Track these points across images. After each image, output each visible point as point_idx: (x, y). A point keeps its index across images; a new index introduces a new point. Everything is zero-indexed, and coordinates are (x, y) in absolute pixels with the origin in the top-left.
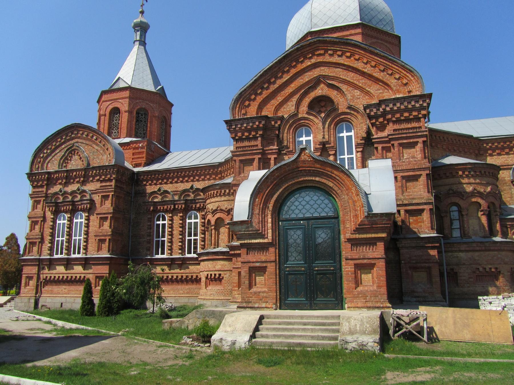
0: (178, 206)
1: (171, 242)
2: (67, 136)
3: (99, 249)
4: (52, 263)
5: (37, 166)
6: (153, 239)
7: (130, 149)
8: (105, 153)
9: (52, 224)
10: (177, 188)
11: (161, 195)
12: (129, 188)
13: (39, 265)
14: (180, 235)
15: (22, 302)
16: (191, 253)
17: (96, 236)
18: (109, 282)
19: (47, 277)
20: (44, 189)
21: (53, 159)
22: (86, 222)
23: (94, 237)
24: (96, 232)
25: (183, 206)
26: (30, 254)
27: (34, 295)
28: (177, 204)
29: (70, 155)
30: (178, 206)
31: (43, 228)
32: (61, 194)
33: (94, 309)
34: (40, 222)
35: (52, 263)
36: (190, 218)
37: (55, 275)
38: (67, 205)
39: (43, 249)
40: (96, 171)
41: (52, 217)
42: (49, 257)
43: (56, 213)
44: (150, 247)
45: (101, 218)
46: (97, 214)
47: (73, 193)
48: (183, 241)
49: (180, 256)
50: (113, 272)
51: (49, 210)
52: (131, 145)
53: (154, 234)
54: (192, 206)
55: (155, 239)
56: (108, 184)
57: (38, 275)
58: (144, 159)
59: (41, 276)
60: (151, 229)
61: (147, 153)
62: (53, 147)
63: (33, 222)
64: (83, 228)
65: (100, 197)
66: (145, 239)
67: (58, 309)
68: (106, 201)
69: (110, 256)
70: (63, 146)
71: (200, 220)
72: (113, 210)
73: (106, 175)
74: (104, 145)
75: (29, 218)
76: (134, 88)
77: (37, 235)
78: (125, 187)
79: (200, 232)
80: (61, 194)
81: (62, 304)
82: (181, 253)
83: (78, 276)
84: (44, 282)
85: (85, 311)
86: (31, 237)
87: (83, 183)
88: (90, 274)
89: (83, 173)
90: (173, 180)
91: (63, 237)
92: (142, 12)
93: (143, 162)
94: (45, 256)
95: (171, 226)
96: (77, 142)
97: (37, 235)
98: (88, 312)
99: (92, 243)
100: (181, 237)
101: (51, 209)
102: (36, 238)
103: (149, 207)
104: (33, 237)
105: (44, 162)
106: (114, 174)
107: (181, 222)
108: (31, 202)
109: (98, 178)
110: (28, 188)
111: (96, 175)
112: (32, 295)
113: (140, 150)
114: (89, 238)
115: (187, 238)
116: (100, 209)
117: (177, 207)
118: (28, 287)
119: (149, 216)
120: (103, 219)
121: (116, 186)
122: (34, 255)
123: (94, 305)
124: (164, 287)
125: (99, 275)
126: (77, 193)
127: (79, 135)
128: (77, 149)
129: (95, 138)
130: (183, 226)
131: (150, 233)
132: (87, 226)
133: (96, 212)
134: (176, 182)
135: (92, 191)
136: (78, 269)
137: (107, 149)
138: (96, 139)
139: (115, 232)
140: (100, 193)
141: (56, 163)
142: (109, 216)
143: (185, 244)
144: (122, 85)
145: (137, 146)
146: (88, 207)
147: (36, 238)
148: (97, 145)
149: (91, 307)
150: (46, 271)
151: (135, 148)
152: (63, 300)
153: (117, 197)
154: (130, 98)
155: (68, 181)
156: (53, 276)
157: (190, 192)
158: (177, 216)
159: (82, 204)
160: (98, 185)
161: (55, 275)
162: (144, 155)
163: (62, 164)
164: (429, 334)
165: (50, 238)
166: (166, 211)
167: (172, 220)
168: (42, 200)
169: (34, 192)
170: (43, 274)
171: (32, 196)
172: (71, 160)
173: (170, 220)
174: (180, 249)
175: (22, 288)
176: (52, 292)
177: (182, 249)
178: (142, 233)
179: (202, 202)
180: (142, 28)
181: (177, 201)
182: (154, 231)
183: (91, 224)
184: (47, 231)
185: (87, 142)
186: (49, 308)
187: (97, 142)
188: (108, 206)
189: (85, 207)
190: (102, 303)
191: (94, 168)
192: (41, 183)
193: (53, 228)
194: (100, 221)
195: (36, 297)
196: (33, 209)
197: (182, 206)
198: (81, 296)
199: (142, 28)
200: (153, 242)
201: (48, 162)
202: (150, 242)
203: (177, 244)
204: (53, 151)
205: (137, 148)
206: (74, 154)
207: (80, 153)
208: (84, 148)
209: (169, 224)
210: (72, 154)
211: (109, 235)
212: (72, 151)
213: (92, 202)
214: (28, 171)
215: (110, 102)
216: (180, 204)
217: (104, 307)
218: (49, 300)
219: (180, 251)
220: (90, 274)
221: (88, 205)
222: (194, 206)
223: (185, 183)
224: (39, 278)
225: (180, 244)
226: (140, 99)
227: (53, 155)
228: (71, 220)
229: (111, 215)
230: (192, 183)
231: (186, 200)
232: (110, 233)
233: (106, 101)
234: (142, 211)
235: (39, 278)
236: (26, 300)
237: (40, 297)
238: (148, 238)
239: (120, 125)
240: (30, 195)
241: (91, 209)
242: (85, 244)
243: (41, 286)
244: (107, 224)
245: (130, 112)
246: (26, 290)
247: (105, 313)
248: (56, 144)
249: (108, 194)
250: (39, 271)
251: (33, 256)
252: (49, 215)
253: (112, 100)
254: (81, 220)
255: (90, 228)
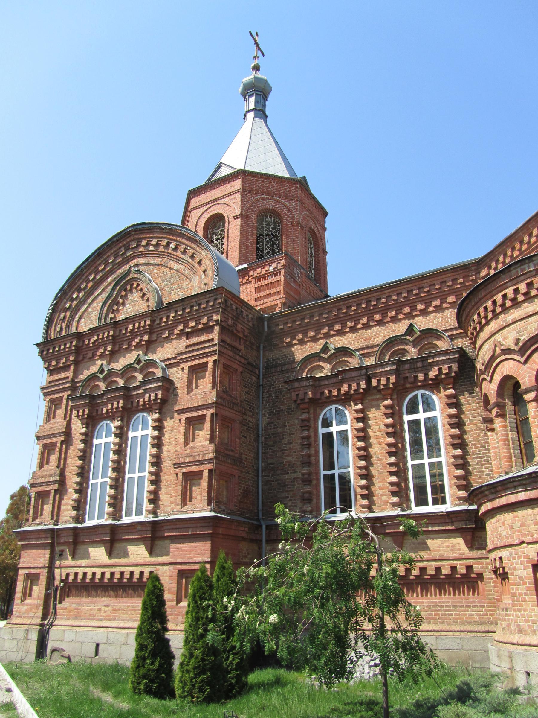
0: (379, 381)
1: (366, 475)
2: (116, 256)
3: (186, 498)
4: (77, 540)
5: (58, 329)
6: (318, 473)
7: (248, 282)
8: (195, 274)
9: (82, 446)
10: (368, 339)
11: (328, 360)
12: (250, 349)
13: (52, 546)
14: (391, 454)
15: (12, 639)
16: (426, 504)
17: (177, 465)
18: (211, 587)
19: (68, 575)
20: (70, 374)
21: (90, 310)
22: (156, 433)
23: (173, 470)
24: (178, 455)
25: (393, 379)
26: (37, 521)
27: (39, 621)
28: (375, 375)
29: (123, 293)
30: (379, 381)
31: (65, 459)
32: (101, 376)
33: (169, 672)
34: (59, 445)
35: (77, 540)
36: (413, 410)
37: (86, 570)
38: (115, 398)
39: (63, 508)
40: (176, 312)
41: (84, 430)
42: (73, 525)
43: (92, 422)
44: (310, 493)
45: (189, 421)
46: (181, 412)
47: (129, 368)
48: (400, 471)
49: (398, 512)
50: (222, 555)
51: (78, 416)
52: (251, 273)
53: (318, 461)
54: (416, 377)
55: (323, 473)
56: (203, 338)
57: (51, 568)
58: (282, 295)
59: (57, 572)
60: (309, 446)
61: (287, 285)
62: (90, 284)
63: (45, 446)
64: (150, 450)
65: (186, 370)
66: (298, 475)
67: (89, 660)
68: (200, 381)
69: (213, 514)
71: (442, 410)
72: (218, 396)
73: (197, 321)
74: (192, 257)
75: (39, 438)
76: (250, 173)
77: (51, 475)
78: (242, 347)
79: (446, 445)
80: (101, 376)
81: (98, 645)
82: (399, 505)
83: (137, 571)
84: (62, 589)
85: (144, 677)
86: (40, 481)
87: (149, 346)
88: (167, 566)
89: (148, 322)
90: (357, 322)
91: (104, 475)
92: (257, 68)
93: (279, 302)
94: (67, 522)
95: (363, 435)
96: (137, 265)
97: (51, 475)
98: (152, 681)
99: (169, 486)
100: (393, 459)
101: (81, 413)
102: (50, 483)
103: (301, 393)
105: (72, 317)
106: (217, 313)
107: (389, 421)
108: (43, 404)
109: (181, 327)
110: (38, 373)
111: (176, 323)
112: (34, 621)
113: (270, 280)
114: (161, 474)
115: (410, 463)
116: (184, 399)
117: (374, 382)
118: (28, 601)
119: (304, 416)
120: (194, 423)
121: (222, 341)
122: (45, 523)
123: (169, 656)
124: (412, 598)
125: (186, 567)
126: (135, 369)
127: (142, 249)
129: (172, 246)
130: (395, 431)
131: (309, 456)
132: (158, 444)
133: (176, 408)
134: (367, 326)
135: (169, 359)
136: (138, 553)
137: (200, 263)
138: (176, 249)
139: (221, 454)
140: (184, 361)
141: (95, 315)
142: (208, 413)
143: (406, 480)
144: (224, 172)
145: (263, 272)
146: (159, 396)
147: (50, 483)
148: (178, 260)
149: (161, 666)
150: (69, 561)
151: (258, 279)
152: (99, 635)
153: (225, 369)
154: (243, 190)
155: (117, 348)
156: (81, 571)
157: (406, 343)
158: (378, 408)
159: (146, 391)
160: (181, 345)
161: (86, 570)
162: (281, 288)
163: (107, 315)
164: (472, 659)
165: (78, 479)
166: (346, 400)
167: (363, 419)
168: (65, 397)
169: (50, 382)
170: (60, 567)
171: (46, 391)
172: (123, 304)
173: (358, 420)
174: (394, 494)
175: (17, 601)
176: (77, 614)
177: (399, 491)
178: (289, 459)
179: (444, 362)
180: (259, 91)
181: (375, 366)
182: (317, 452)
183: (166, 438)
184: (74, 464)
185: (158, 260)
186: (69, 658)
187: (179, 254)
188: (205, 391)
189: (153, 398)
190: (191, 655)
191: (170, 305)
192: (64, 360)
193: (85, 456)
194: (186, 429)
195: (42, 625)
196: (48, 419)
197: (388, 379)
198: (136, 624)
199: (259, 91)
200: (318, 480)
201: (80, 318)
202: (310, 479)
203: (383, 482)
205: (264, 277)
206: (131, 290)
207: (141, 286)
208: (151, 273)
209: (358, 430)
210: (125, 290)
211: (209, 461)
212: (126, 285)
213: (168, 384)
214: (40, 339)
215: (205, 208)
216: (382, 374)
217: (200, 670)
218: (69, 634)
219: (396, 499)
220: (167, 566)
221: (160, 393)
222: (421, 377)
223: (391, 325)
224: (51, 577)
225: (394, 479)
226: (262, 193)
227: (89, 301)
228: (122, 434)
229: (213, 411)
230: (407, 322)
231: (400, 363)
232: (211, 455)
233: (197, 208)
234: (284, 407)
235: (51, 577)
236: (21, 634)
237: (52, 625)
238: (306, 470)
239: (225, 247)
240: (43, 388)
241: (163, 406)
242: (152, 488)
243: (55, 600)
244: (203, 435)
245: (244, 217)
246: (24, 608)
247: (201, 690)
248: (95, 278)
249: (204, 360)
250: (52, 561)
251: (41, 524)
252: (78, 428)
253: (207, 203)
254: (145, 432)
255: (164, 448)
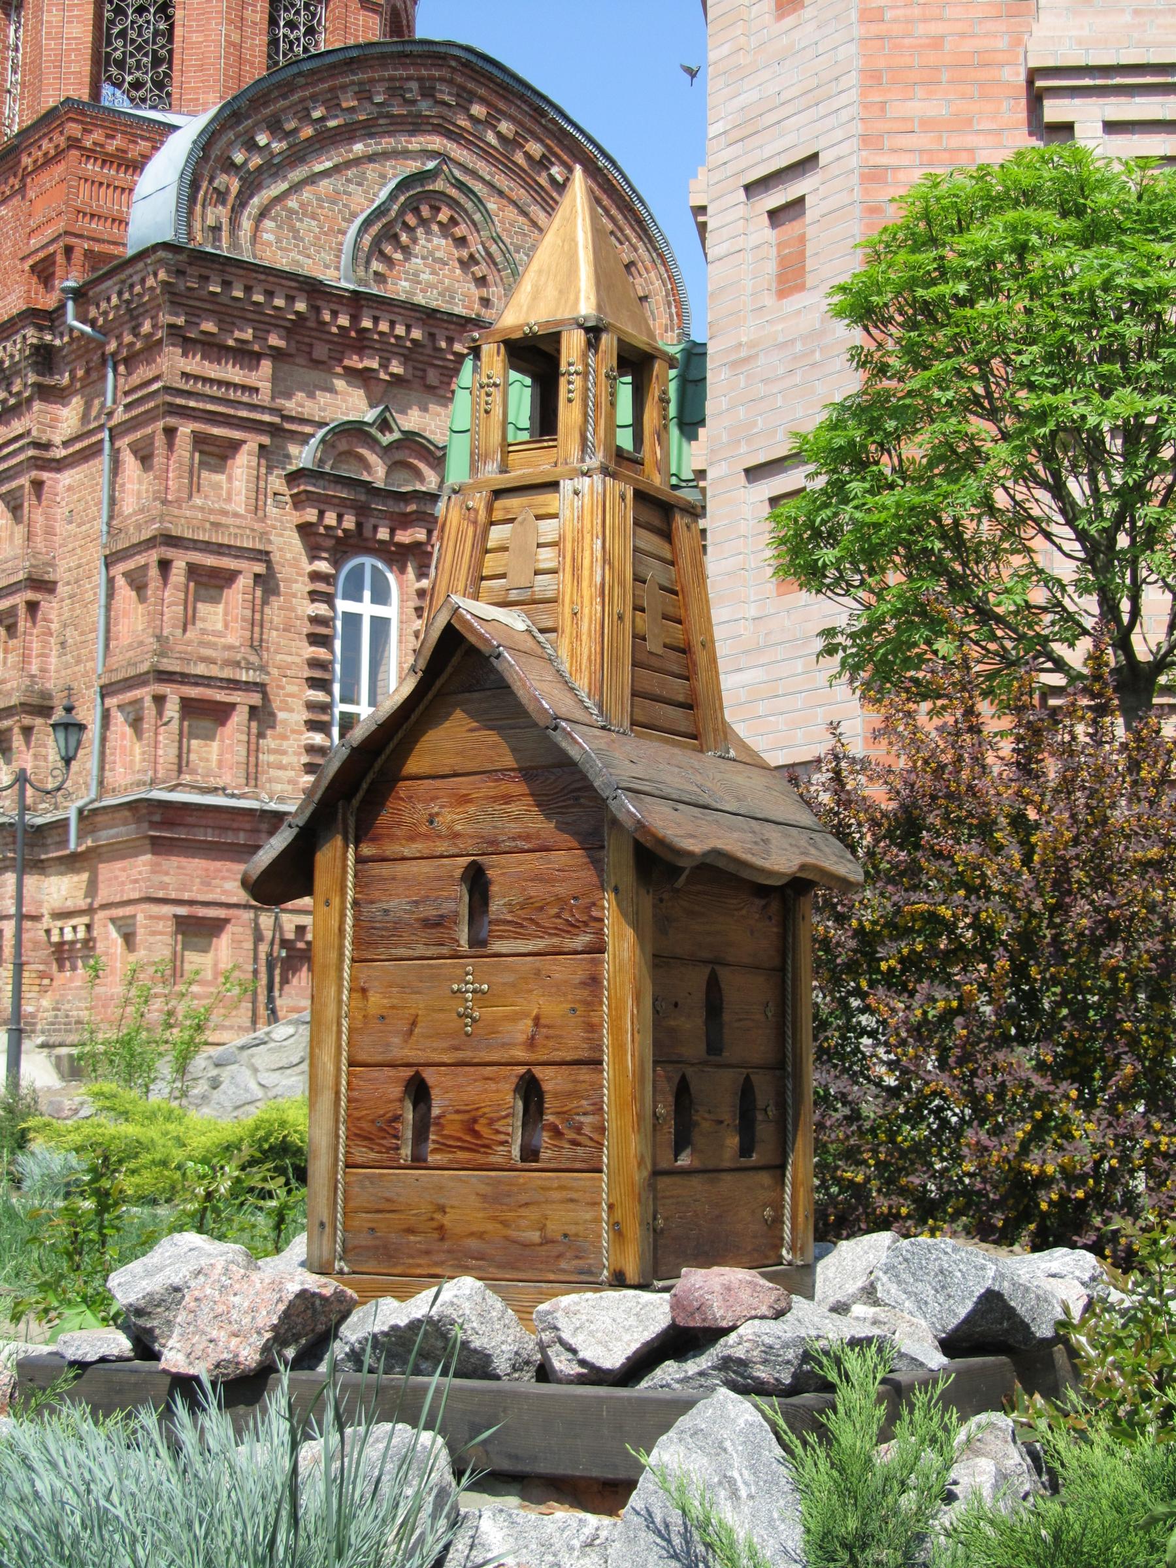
21: (292, 203)
70: (359, 148)
77: (228, 663)
104: (214, 671)
128: (454, 204)
201: (263, 214)
204: (298, 155)
227: (296, 175)
